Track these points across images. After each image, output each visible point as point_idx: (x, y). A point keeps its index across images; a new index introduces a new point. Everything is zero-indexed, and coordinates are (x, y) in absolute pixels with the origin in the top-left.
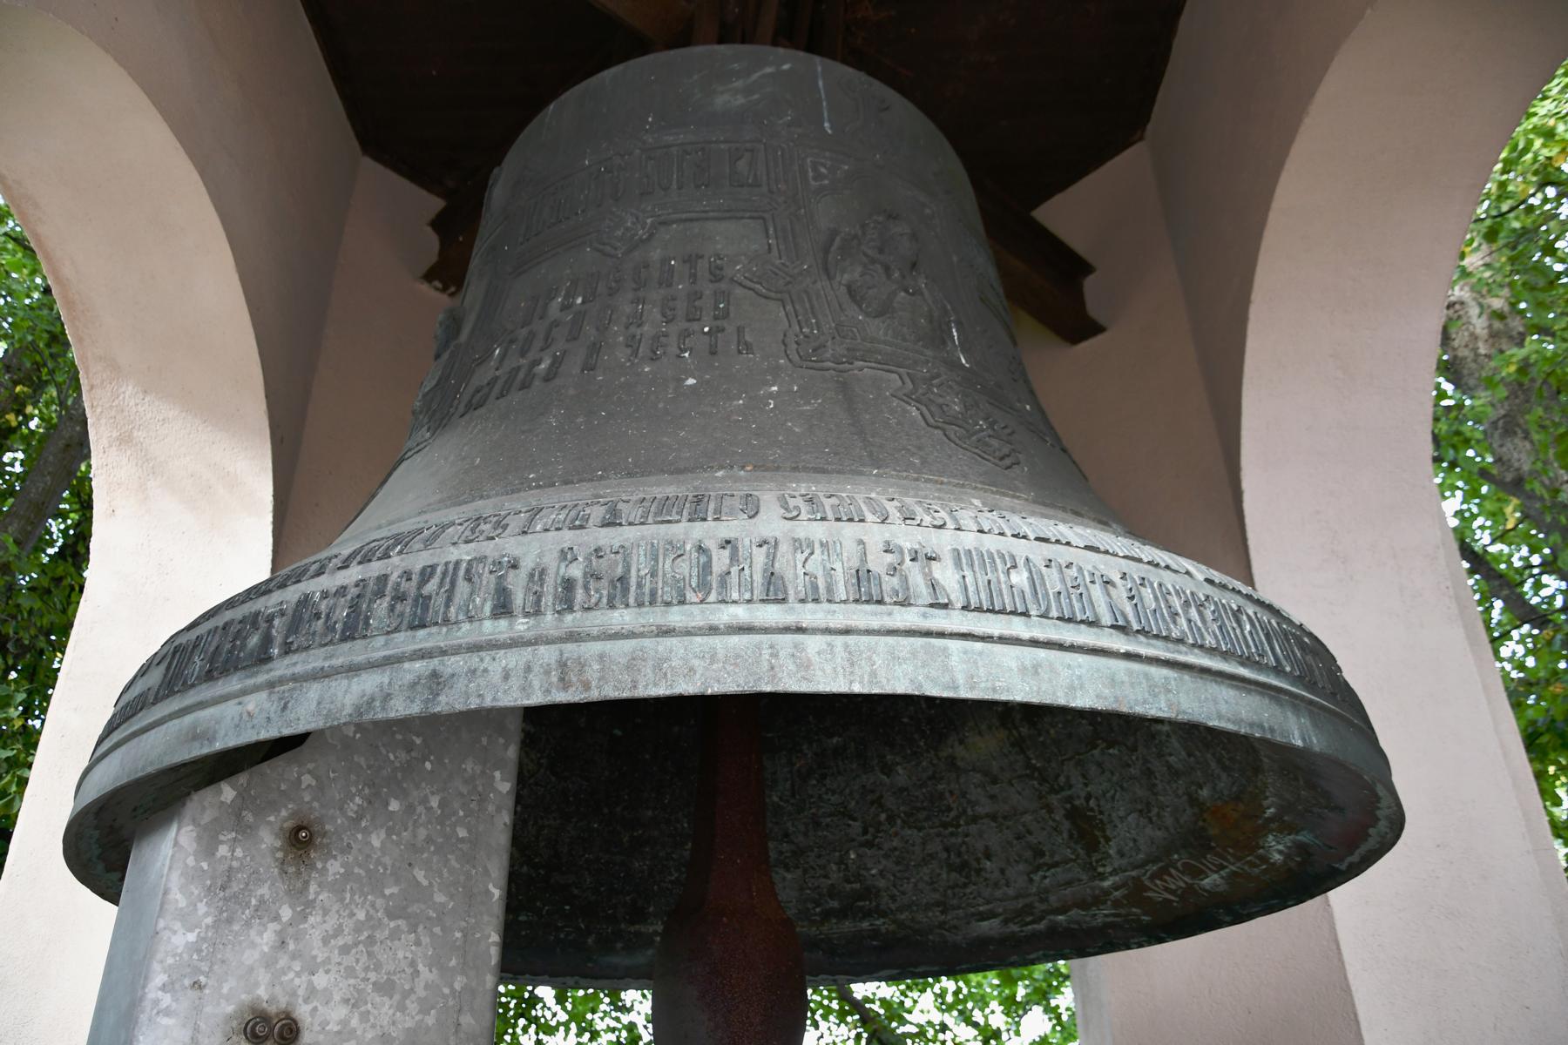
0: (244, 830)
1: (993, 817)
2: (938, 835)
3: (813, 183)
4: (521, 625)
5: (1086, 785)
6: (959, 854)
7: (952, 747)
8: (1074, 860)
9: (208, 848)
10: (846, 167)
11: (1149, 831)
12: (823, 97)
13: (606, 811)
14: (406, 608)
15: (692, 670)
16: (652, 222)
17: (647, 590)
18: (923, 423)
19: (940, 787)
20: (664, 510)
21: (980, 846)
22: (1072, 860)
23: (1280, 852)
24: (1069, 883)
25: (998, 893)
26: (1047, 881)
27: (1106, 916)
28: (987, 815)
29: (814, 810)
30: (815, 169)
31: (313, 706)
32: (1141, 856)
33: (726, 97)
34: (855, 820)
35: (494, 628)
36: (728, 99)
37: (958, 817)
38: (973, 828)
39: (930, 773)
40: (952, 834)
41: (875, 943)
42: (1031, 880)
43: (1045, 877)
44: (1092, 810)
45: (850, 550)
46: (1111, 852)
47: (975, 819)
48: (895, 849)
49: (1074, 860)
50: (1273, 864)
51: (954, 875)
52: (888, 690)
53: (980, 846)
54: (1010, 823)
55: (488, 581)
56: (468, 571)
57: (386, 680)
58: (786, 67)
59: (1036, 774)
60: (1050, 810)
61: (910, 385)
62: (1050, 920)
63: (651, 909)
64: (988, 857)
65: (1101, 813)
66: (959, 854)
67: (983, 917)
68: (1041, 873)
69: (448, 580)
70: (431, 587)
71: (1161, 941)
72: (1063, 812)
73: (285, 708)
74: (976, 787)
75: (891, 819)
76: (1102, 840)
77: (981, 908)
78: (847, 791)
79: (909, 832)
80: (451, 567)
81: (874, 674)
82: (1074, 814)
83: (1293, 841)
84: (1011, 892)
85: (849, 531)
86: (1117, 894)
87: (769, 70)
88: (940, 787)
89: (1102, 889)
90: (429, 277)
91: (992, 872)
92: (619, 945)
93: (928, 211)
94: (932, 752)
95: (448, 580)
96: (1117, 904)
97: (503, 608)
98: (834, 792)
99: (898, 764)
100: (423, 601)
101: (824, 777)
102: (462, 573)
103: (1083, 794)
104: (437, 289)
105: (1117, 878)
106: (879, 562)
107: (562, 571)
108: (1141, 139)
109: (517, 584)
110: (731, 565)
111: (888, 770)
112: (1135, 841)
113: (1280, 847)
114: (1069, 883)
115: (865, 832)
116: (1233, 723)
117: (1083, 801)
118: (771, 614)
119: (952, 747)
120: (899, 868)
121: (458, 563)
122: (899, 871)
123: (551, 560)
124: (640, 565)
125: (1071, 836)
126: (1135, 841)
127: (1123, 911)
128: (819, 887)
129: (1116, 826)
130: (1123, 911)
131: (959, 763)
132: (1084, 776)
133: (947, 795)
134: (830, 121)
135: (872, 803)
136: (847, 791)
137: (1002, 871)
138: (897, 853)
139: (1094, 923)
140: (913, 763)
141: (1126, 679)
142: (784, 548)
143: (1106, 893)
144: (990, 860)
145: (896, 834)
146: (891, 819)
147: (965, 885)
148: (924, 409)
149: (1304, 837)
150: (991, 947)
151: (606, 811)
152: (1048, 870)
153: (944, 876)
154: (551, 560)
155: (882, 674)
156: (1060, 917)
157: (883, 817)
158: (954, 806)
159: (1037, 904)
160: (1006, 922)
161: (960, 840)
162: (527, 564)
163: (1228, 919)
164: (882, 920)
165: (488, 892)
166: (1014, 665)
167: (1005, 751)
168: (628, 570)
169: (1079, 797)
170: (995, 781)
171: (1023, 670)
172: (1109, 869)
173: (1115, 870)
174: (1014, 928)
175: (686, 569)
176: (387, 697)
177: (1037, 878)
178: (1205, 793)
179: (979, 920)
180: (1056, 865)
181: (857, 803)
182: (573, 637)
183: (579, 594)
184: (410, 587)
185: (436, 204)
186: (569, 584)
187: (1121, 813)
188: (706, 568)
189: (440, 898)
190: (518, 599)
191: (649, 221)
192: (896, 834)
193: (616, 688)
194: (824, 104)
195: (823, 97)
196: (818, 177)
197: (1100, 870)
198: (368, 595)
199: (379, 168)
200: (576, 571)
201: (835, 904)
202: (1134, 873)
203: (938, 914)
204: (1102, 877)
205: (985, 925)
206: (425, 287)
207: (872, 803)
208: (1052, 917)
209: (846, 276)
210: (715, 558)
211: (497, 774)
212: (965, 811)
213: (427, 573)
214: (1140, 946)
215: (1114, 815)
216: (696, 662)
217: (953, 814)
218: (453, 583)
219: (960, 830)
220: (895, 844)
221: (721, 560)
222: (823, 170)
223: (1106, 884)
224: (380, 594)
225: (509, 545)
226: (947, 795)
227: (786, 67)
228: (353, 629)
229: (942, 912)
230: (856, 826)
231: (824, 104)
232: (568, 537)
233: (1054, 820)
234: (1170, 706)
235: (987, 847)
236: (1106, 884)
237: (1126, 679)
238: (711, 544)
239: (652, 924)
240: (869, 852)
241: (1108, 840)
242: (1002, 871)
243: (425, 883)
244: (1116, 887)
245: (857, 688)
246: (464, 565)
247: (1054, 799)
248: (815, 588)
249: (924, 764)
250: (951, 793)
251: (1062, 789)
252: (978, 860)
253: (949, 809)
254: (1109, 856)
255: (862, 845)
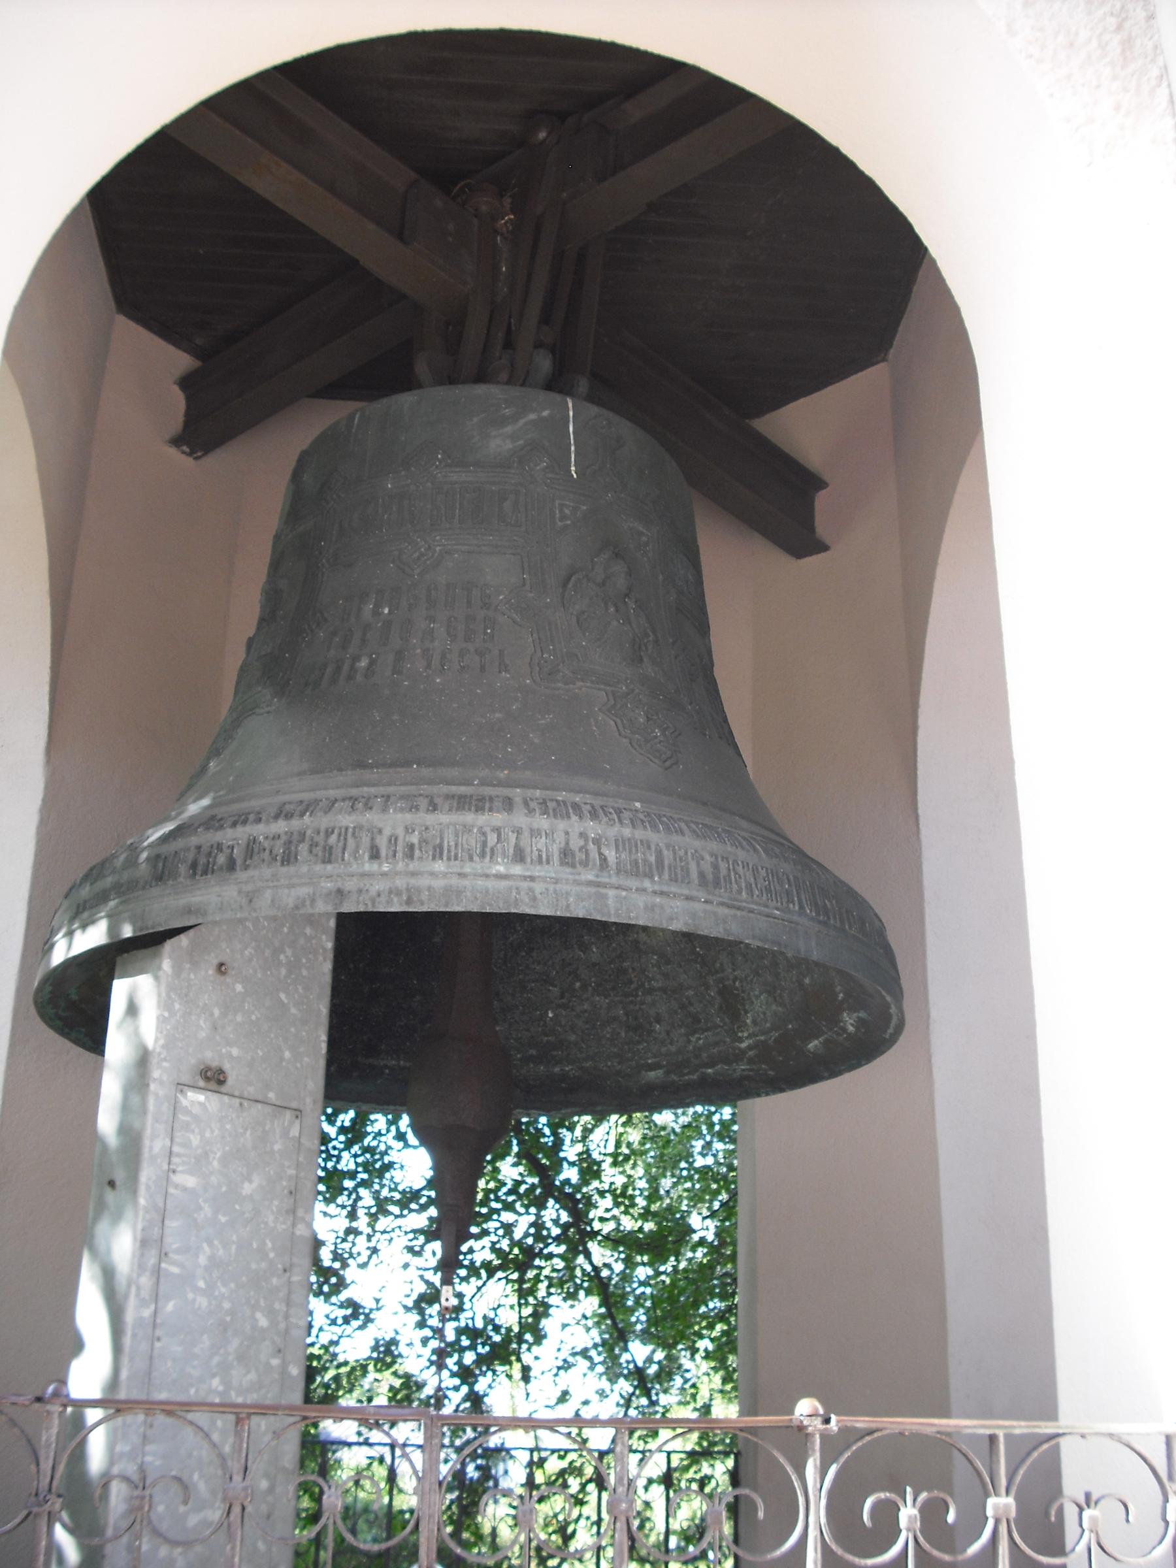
0: (195, 965)
1: (664, 990)
2: (621, 1002)
3: (560, 524)
4: (386, 867)
5: (734, 970)
6: (636, 1018)
7: (637, 933)
8: (722, 1027)
9: (178, 970)
10: (585, 508)
11: (774, 1007)
12: (572, 442)
13: (351, 966)
14: (318, 850)
15: (476, 898)
16: (440, 550)
17: (453, 854)
18: (617, 734)
19: (626, 964)
20: (462, 803)
21: (652, 1012)
22: (720, 1026)
23: (852, 1025)
24: (717, 1044)
25: (664, 1050)
26: (701, 1042)
27: (743, 1070)
28: (660, 989)
29: (521, 977)
30: (561, 511)
31: (269, 901)
32: (768, 1025)
33: (498, 441)
34: (555, 986)
35: (374, 867)
36: (500, 443)
37: (637, 989)
38: (649, 999)
39: (619, 952)
40: (631, 1002)
41: (564, 1085)
42: (689, 1041)
43: (699, 1039)
44: (737, 989)
45: (560, 838)
46: (748, 1021)
47: (651, 991)
48: (586, 1011)
49: (722, 1027)
50: (850, 1034)
51: (631, 1034)
52: (574, 915)
53: (652, 1012)
54: (677, 996)
55: (366, 840)
56: (354, 834)
57: (311, 892)
58: (545, 413)
59: (699, 959)
60: (707, 988)
61: (612, 702)
62: (702, 1073)
63: (383, 1047)
64: (658, 1022)
65: (743, 992)
66: (636, 1018)
67: (651, 1068)
68: (697, 1036)
69: (342, 838)
70: (333, 839)
71: (782, 1090)
72: (716, 989)
73: (251, 901)
74: (653, 966)
75: (584, 987)
76: (743, 1012)
77: (650, 1061)
78: (550, 963)
79: (598, 998)
80: (343, 830)
81: (568, 906)
82: (724, 992)
83: (858, 1017)
84: (673, 1049)
85: (561, 825)
86: (751, 1053)
87: (532, 416)
88: (626, 964)
89: (740, 1049)
90: (176, 442)
91: (660, 1033)
92: (355, 1074)
93: (644, 539)
94: (622, 937)
95: (342, 838)
96: (751, 1061)
97: (375, 855)
98: (539, 963)
99: (593, 943)
100: (329, 850)
101: (532, 950)
102: (350, 834)
103: (731, 977)
104: (184, 452)
105: (751, 1041)
106: (576, 843)
107: (407, 839)
108: (884, 360)
109: (382, 842)
110: (498, 842)
111: (584, 947)
112: (764, 1014)
113: (852, 1021)
114: (717, 1044)
115: (562, 996)
116: (760, 940)
117: (731, 982)
118: (517, 870)
119: (637, 933)
120: (587, 1026)
121: (347, 829)
122: (588, 1029)
123: (400, 832)
124: (449, 840)
125: (721, 1008)
126: (764, 1014)
127: (755, 1067)
128: (521, 1038)
129: (753, 1003)
130: (755, 1067)
131: (642, 947)
132: (733, 964)
133: (630, 970)
134: (575, 465)
135: (570, 974)
136: (550, 963)
137: (668, 1033)
138: (586, 1015)
139: (735, 1075)
140: (606, 944)
141: (702, 915)
142: (526, 834)
143: (743, 1052)
144: (659, 1024)
145: (587, 999)
146: (584, 987)
147: (639, 1043)
148: (619, 721)
149: (862, 1014)
150: (656, 1093)
151: (351, 966)
152: (703, 1033)
153: (623, 1034)
154: (400, 832)
155: (572, 908)
156: (710, 1070)
157: (578, 984)
158: (635, 980)
159: (692, 1060)
160: (668, 1073)
161: (637, 1007)
162: (387, 832)
163: (826, 1074)
164: (571, 1067)
165: (320, 1010)
166: (641, 904)
167: (677, 940)
168: (442, 839)
169: (728, 979)
170: (668, 962)
171: (646, 908)
172: (745, 1034)
173: (749, 1035)
174: (674, 1077)
175: (473, 841)
176: (313, 901)
177: (693, 1039)
178: (807, 981)
179: (646, 1071)
180: (707, 1030)
181: (557, 972)
182: (414, 874)
183: (417, 853)
184: (320, 839)
185: (182, 361)
186: (411, 847)
187: (757, 993)
188: (484, 844)
189: (293, 1011)
190: (383, 853)
191: (438, 549)
192: (587, 999)
193: (436, 905)
194: (573, 448)
195: (572, 442)
196: (563, 517)
197: (740, 1034)
198: (295, 842)
199: (132, 325)
200: (415, 839)
201: (533, 1052)
202: (762, 1038)
203: (615, 1064)
204: (741, 1040)
205: (652, 1074)
206: (172, 451)
207: (570, 974)
208: (704, 1070)
209: (577, 607)
210: (489, 838)
211: (324, 937)
212: (643, 985)
213: (329, 833)
214: (767, 1094)
215: (752, 993)
216: (478, 895)
217: (633, 986)
218: (345, 839)
219: (638, 999)
220: (585, 1007)
221: (492, 839)
222: (567, 511)
223: (744, 1045)
224: (302, 840)
225: (372, 818)
226: (630, 970)
227: (545, 413)
228: (288, 858)
229: (619, 1063)
230: (555, 991)
231: (573, 448)
232: (409, 817)
233: (710, 995)
234: (725, 930)
235: (658, 1014)
236: (744, 1045)
237: (702, 915)
238: (487, 830)
239: (383, 1059)
240: (564, 1013)
241: (746, 1012)
242: (668, 1033)
243: (286, 1001)
244: (750, 1048)
245: (559, 914)
246: (350, 830)
247: (711, 980)
248: (540, 856)
249: (614, 945)
250: (633, 969)
251: (717, 972)
252: (650, 1023)
253: (631, 982)
254: (746, 1024)
255: (559, 1006)
